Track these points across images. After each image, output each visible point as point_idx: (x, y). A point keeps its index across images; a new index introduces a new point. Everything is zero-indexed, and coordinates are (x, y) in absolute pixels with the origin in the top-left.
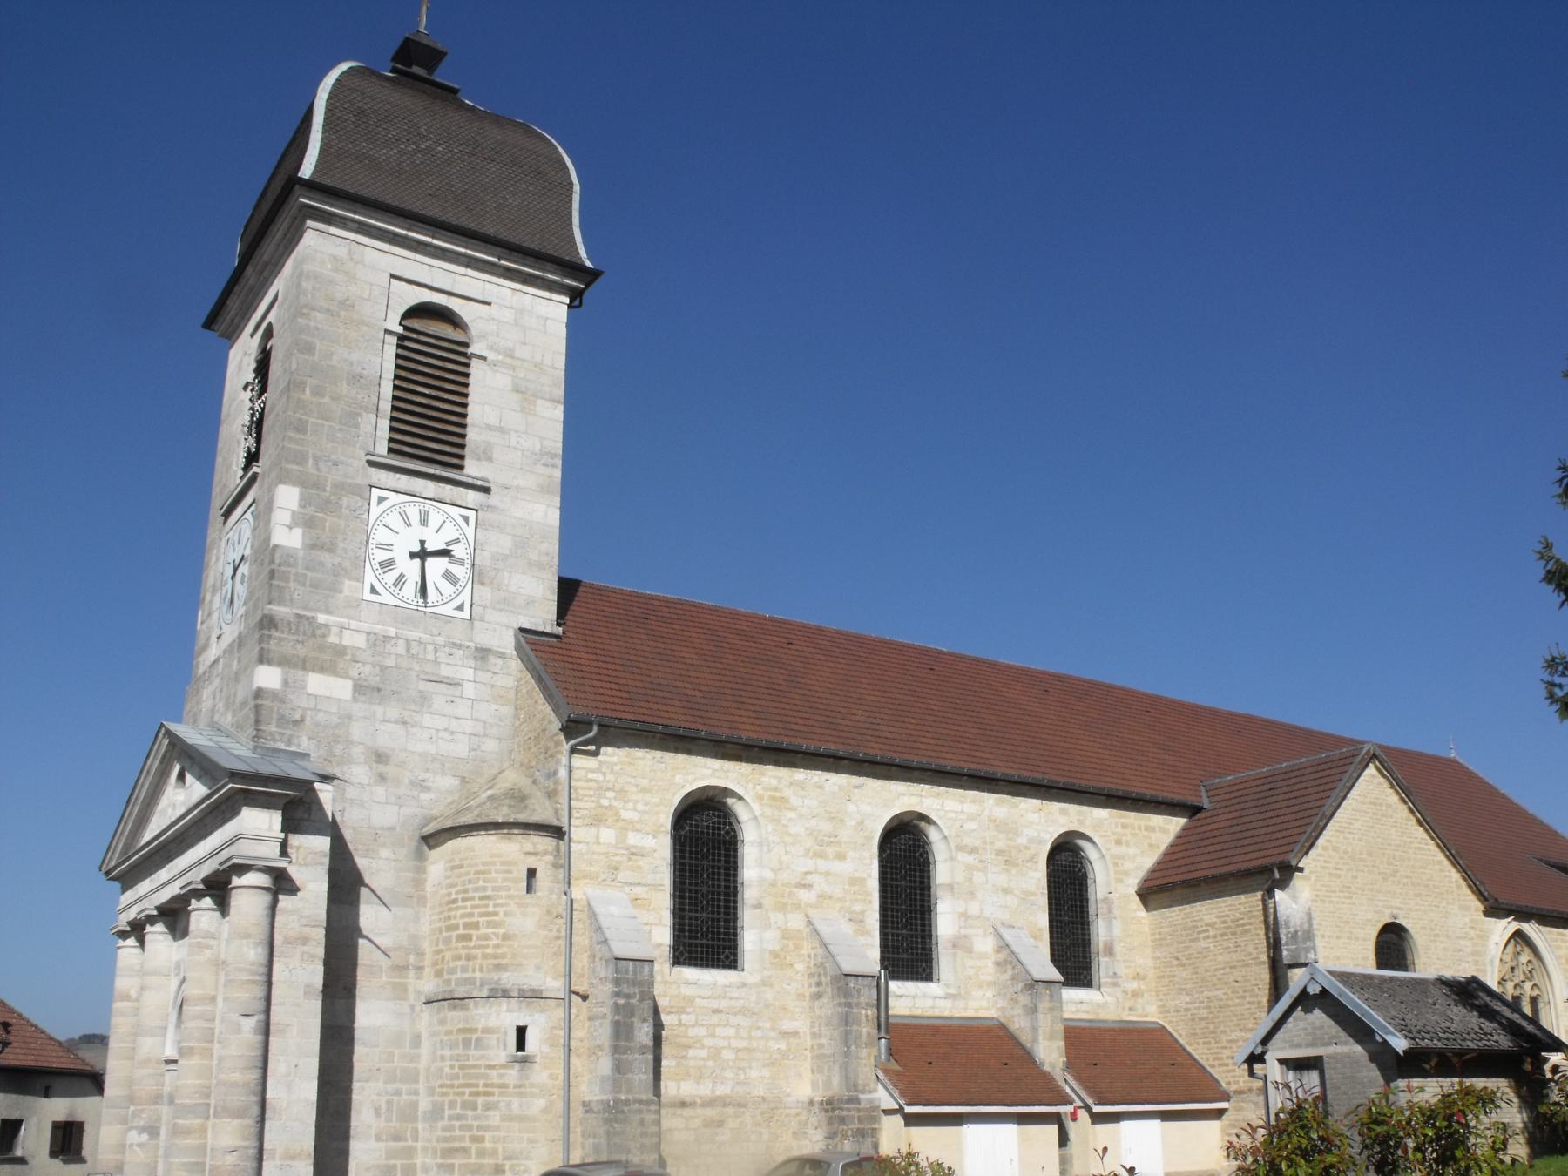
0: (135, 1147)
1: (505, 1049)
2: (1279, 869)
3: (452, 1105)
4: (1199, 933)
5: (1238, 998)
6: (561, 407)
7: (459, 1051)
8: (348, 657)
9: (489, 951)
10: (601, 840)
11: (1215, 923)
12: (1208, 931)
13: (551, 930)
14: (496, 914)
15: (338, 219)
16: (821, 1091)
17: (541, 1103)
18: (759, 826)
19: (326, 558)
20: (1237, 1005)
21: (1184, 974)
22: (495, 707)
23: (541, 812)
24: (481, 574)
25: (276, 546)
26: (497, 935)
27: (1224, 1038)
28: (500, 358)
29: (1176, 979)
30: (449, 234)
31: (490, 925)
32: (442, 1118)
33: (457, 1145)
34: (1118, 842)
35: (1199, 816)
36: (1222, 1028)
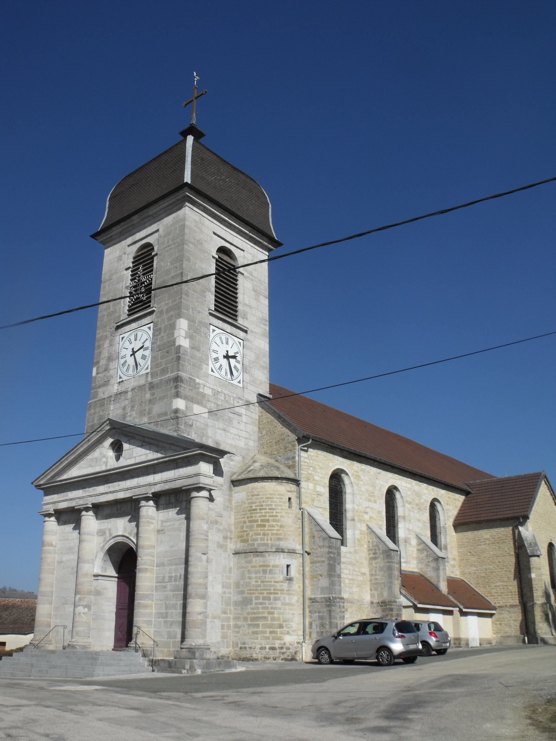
0: (82, 614)
1: (282, 574)
2: (523, 518)
3: (257, 598)
4: (481, 542)
5: (500, 569)
6: (267, 300)
7: (261, 574)
8: (206, 399)
9: (274, 532)
10: (309, 488)
11: (489, 538)
12: (486, 541)
13: (297, 525)
14: (277, 516)
15: (197, 204)
16: (376, 598)
17: (295, 598)
18: (352, 486)
19: (197, 353)
20: (499, 572)
21: (473, 559)
22: (252, 427)
23: (292, 476)
24: (246, 368)
25: (180, 346)
26: (277, 525)
27: (493, 585)
28: (248, 275)
29: (470, 561)
30: (235, 218)
31: (274, 521)
32: (251, 604)
33: (260, 615)
34: (447, 504)
35: (469, 496)
36: (492, 581)
